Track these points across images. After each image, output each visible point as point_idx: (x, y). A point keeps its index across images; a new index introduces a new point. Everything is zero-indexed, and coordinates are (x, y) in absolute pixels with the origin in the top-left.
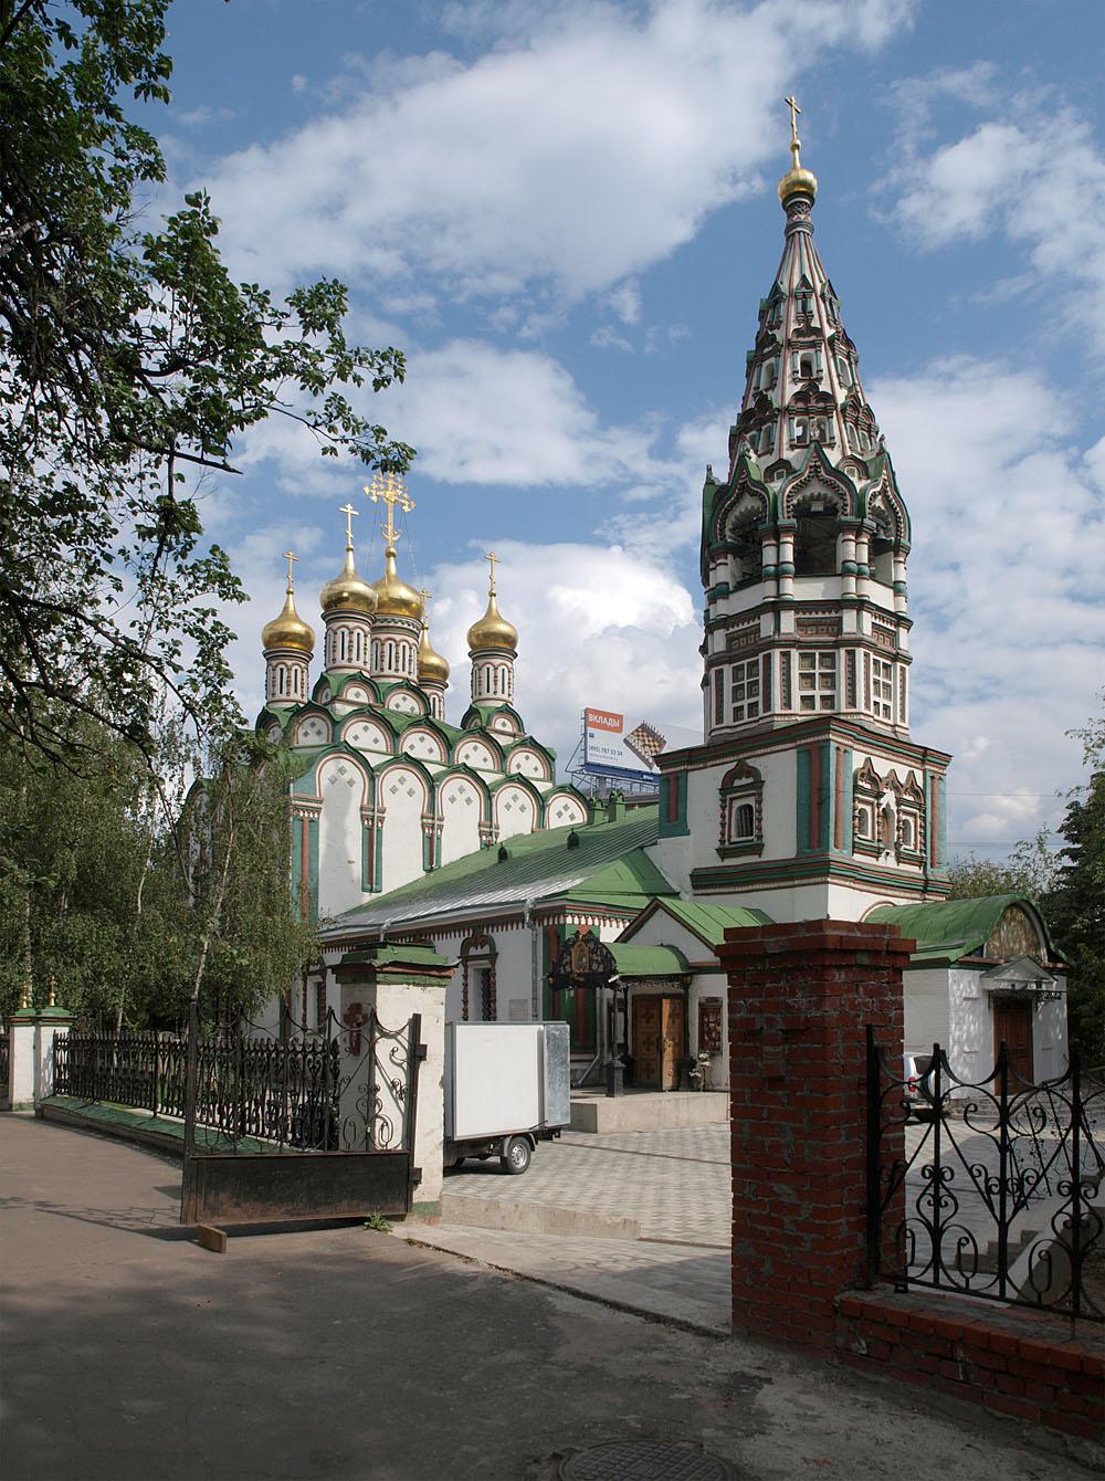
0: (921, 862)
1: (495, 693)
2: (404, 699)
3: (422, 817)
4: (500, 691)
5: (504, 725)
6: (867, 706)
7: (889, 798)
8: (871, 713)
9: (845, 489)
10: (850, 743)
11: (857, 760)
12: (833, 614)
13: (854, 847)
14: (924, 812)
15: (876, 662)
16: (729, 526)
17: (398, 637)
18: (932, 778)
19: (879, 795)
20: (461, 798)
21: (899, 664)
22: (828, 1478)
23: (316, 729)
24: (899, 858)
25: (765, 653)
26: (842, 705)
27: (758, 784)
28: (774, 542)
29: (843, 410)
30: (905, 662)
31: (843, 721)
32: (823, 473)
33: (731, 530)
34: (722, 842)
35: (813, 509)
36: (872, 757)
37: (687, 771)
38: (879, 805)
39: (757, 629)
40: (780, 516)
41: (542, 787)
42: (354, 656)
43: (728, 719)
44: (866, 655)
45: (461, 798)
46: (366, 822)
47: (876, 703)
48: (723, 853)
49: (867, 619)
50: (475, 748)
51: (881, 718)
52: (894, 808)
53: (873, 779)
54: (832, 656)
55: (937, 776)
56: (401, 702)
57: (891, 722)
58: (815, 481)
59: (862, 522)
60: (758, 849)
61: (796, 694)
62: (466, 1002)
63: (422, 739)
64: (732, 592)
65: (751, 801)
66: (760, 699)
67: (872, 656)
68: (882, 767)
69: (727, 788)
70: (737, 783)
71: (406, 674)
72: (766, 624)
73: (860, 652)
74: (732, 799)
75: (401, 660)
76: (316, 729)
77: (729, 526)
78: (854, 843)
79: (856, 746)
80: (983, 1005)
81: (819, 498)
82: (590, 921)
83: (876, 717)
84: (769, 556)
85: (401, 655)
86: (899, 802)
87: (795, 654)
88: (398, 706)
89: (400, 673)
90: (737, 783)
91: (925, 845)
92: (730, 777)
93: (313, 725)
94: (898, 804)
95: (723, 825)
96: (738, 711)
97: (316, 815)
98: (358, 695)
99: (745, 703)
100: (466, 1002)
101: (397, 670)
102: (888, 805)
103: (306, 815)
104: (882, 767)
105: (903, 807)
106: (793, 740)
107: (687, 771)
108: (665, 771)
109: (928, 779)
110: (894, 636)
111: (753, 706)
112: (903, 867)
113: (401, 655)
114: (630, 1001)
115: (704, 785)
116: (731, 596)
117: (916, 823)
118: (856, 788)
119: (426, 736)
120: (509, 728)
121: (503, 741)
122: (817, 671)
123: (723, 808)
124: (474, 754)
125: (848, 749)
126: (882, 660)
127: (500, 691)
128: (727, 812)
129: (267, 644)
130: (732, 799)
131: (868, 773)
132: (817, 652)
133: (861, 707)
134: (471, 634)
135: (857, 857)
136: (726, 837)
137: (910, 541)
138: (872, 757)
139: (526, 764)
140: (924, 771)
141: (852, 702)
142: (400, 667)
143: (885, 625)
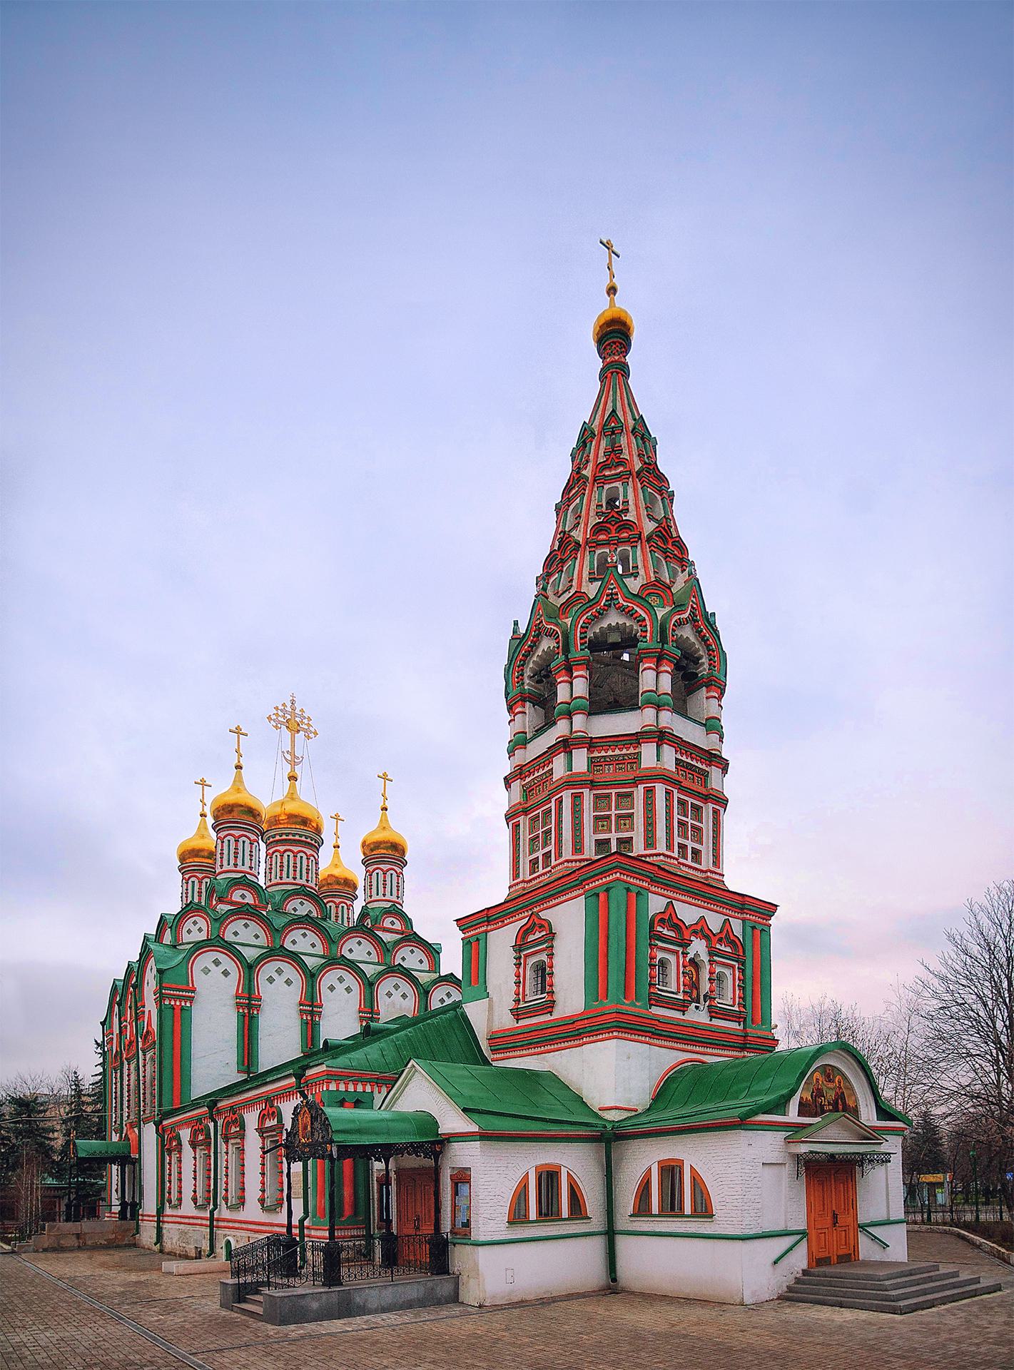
0: (738, 1017)
1: (384, 895)
2: (302, 904)
3: (301, 1004)
4: (388, 893)
5: (393, 923)
6: (670, 846)
7: (698, 947)
8: (676, 855)
9: (644, 615)
10: (645, 884)
11: (656, 904)
12: (632, 750)
13: (650, 1000)
14: (743, 964)
15: (682, 803)
16: (528, 673)
17: (296, 849)
18: (753, 928)
19: (685, 944)
20: (340, 988)
21: (711, 806)
22: (946, 1367)
23: (198, 926)
24: (714, 1013)
25: (557, 797)
26: (638, 848)
27: (551, 935)
28: (566, 678)
29: (649, 539)
30: (717, 803)
31: (648, 862)
32: (621, 601)
33: (530, 677)
34: (517, 1001)
35: (610, 640)
36: (673, 901)
37: (486, 932)
38: (685, 954)
39: (637, 757)
40: (572, 649)
41: (424, 978)
42: (239, 862)
43: (525, 873)
44: (668, 793)
45: (340, 988)
46: (241, 1011)
47: (682, 847)
48: (517, 1014)
49: (669, 755)
50: (397, 987)
51: (689, 862)
52: (704, 957)
53: (677, 925)
54: (630, 795)
55: (759, 927)
56: (299, 907)
57: (703, 867)
58: (613, 611)
59: (662, 649)
60: (549, 1007)
61: (589, 839)
62: (195, 1179)
63: (304, 935)
64: (532, 739)
65: (544, 957)
66: (551, 848)
67: (676, 794)
68: (688, 913)
69: (520, 946)
70: (531, 938)
71: (303, 882)
72: (559, 766)
73: (660, 789)
74: (526, 956)
75: (285, 869)
76: (198, 926)
77: (528, 673)
78: (650, 993)
79: (653, 889)
80: (787, 1171)
81: (617, 628)
82: (360, 1088)
83: (681, 860)
84: (562, 693)
85: (298, 865)
86: (712, 952)
87: (588, 795)
88: (295, 910)
89: (298, 881)
90: (531, 938)
91: (744, 999)
92: (524, 932)
93: (195, 923)
94: (711, 954)
95: (517, 984)
96: (534, 863)
97: (188, 1004)
98: (243, 896)
99: (539, 854)
100: (263, 1174)
101: (236, 865)
102: (697, 955)
103: (178, 1003)
104: (688, 913)
105: (715, 958)
106: (580, 885)
107: (486, 932)
108: (467, 935)
109: (749, 930)
110: (705, 775)
111: (547, 856)
112: (716, 1022)
113: (298, 865)
114: (393, 1175)
115: (502, 941)
116: (528, 746)
117: (734, 976)
118: (654, 936)
119: (308, 932)
120: (398, 926)
121: (387, 937)
122: (613, 812)
123: (518, 965)
124: (358, 950)
125: (642, 891)
126: (690, 800)
127: (388, 893)
128: (521, 970)
129: (182, 858)
130: (526, 956)
131: (669, 918)
132: (613, 791)
133: (661, 847)
134: (364, 844)
135: (656, 1011)
136: (521, 997)
137: (725, 677)
138: (673, 901)
139: (411, 959)
140: (744, 920)
141: (650, 841)
142: (298, 877)
143: (694, 763)
